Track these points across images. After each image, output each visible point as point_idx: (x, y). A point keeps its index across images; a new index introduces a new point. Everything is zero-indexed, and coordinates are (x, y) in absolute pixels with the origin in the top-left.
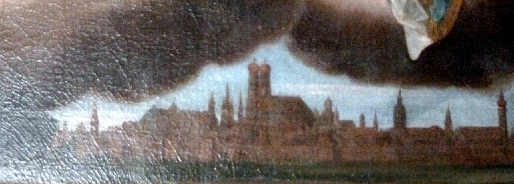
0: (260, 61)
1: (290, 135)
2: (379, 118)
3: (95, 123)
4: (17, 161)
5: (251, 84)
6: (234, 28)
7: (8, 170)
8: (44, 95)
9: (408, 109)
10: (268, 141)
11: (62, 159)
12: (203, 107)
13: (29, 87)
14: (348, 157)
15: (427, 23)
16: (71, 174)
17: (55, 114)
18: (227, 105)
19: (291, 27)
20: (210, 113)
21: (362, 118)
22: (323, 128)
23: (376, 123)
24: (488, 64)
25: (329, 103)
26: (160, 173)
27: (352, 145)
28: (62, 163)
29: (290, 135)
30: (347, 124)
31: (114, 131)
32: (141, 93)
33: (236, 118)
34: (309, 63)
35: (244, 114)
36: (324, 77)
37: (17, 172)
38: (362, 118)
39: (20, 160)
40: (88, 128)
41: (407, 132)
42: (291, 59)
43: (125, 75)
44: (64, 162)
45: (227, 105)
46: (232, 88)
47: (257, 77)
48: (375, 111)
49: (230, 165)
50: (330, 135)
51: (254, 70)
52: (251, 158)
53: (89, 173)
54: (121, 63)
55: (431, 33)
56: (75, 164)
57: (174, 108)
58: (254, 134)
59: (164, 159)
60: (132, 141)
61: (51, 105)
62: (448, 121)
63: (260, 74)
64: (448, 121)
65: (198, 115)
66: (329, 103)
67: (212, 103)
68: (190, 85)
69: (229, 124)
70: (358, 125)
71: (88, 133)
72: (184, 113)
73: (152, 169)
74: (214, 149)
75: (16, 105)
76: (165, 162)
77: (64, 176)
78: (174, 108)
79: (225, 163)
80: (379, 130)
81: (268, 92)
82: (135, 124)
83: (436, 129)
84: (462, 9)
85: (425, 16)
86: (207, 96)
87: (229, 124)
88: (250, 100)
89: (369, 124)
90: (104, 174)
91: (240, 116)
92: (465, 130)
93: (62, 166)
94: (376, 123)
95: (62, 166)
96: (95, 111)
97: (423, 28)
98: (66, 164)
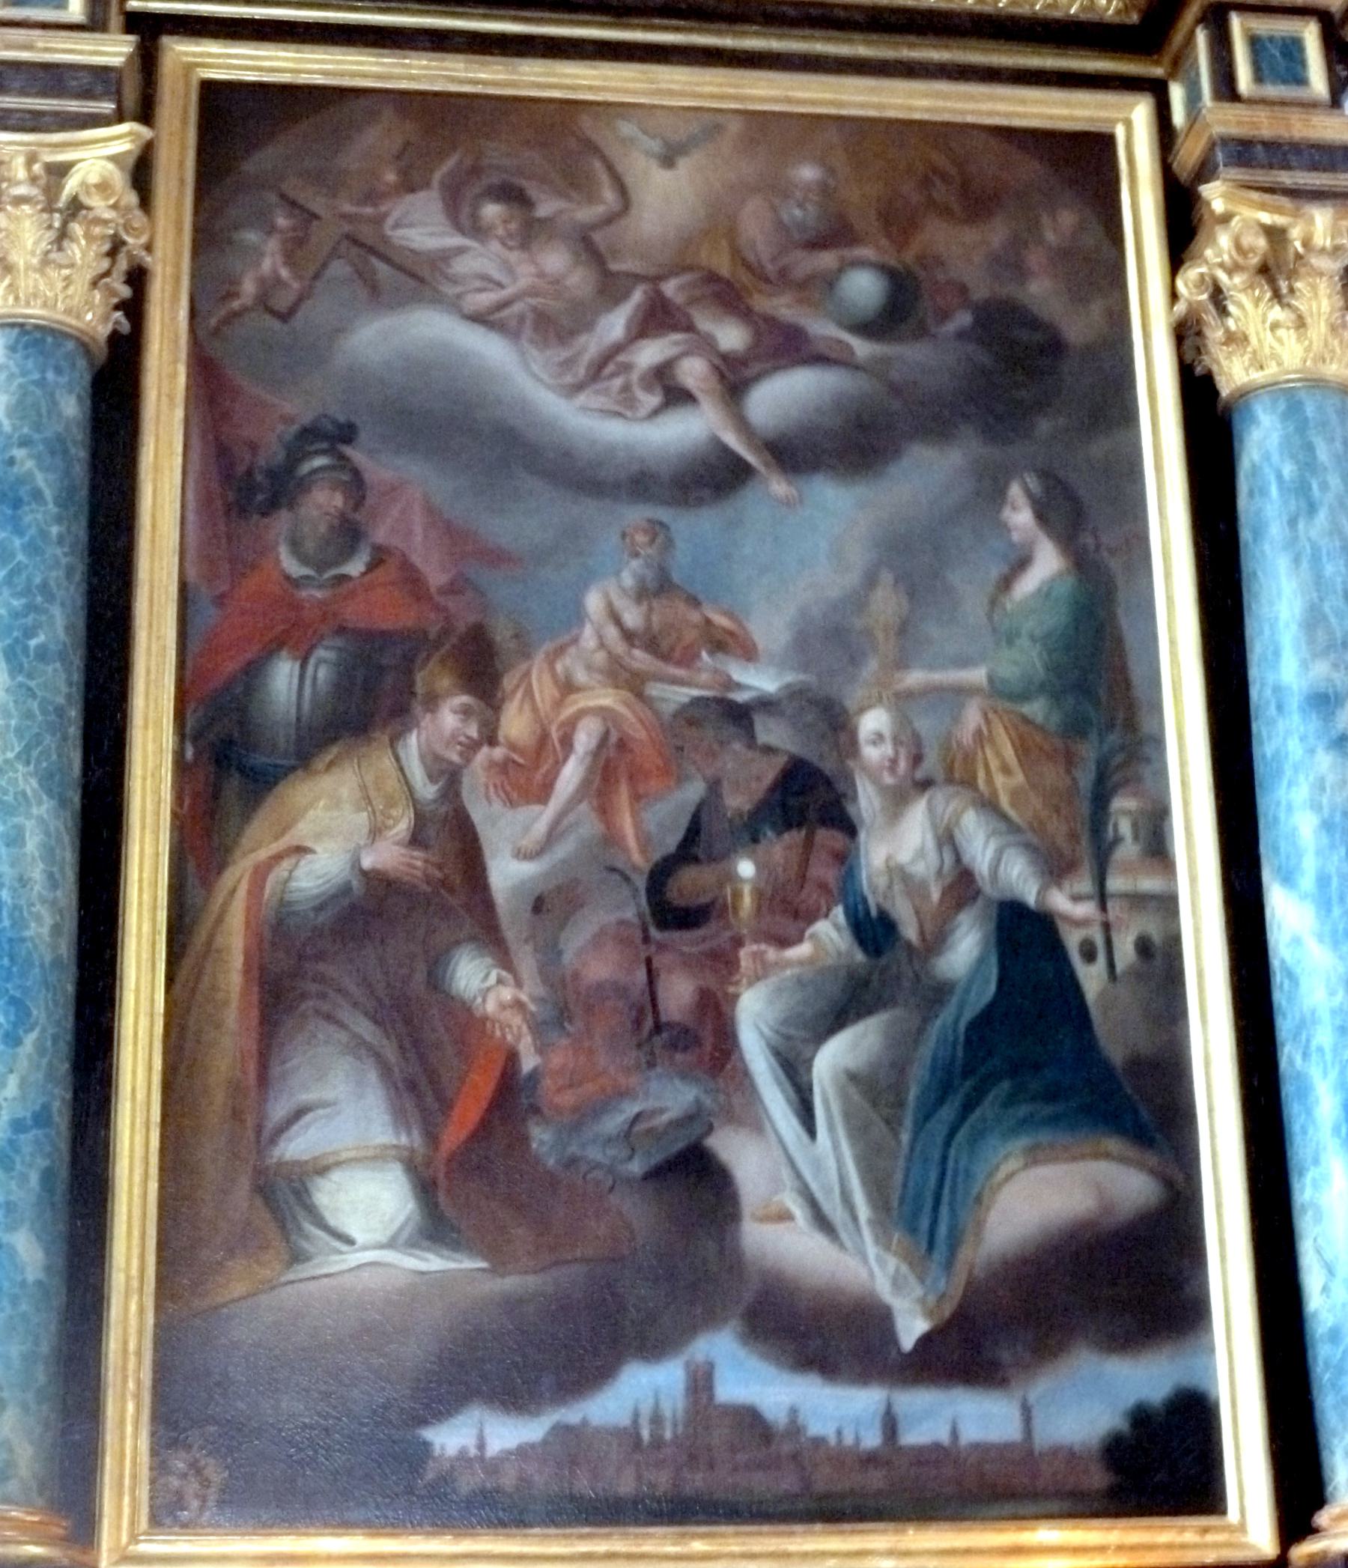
0: (700, 1357)
1: (742, 1457)
2: (862, 1433)
3: (481, 1446)
4: (379, 1499)
5: (687, 1389)
6: (1292, 122)
7: (332, 994)
8: (414, 1409)
9: (900, 1418)
10: (711, 1466)
11: (436, 1496)
12: (625, 1421)
13: (395, 1400)
14: (820, 1486)
15: (922, 1301)
16: (450, 1516)
17: (429, 1434)
18: (656, 1419)
19: (740, 1309)
20: (632, 1431)
21: (839, 1433)
22: (787, 1448)
23: (858, 1439)
24: (1005, 1356)
25: (793, 1411)
26: (567, 1514)
27: (826, 1470)
28: (437, 1500)
29: (742, 1457)
30: (819, 1442)
31: (506, 1455)
32: (795, 693)
33: (668, 1435)
34: (765, 1356)
35: (680, 1429)
36: (786, 1376)
37: (378, 1513)
38: (839, 1433)
39: (384, 1498)
40: (473, 1452)
41: (900, 1450)
42: (741, 1353)
43: (519, 1380)
44: (440, 1499)
45: (656, 1419)
46: (662, 1397)
47: (695, 1381)
48: (857, 1422)
49: (659, 1502)
50: (795, 1457)
51: (692, 1368)
52: (688, 1490)
53: (472, 1514)
54: (515, 1364)
55: (929, 1314)
56: (455, 1502)
57: (585, 1423)
58: (693, 1458)
59: (571, 1494)
60: (531, 1469)
61: (424, 1422)
62: (955, 1434)
63: (700, 1373)
64: (955, 1434)
65: (618, 1433)
66: (793, 1411)
67: (636, 1416)
68: (767, 1060)
69: (657, 1443)
70: (832, 1441)
71: (471, 1459)
72: (597, 1430)
73: (556, 1507)
74: (639, 1478)
75: (377, 1424)
76: (572, 1498)
77: (439, 1519)
78: (585, 1423)
79: (653, 1498)
80: (861, 1449)
81: (711, 1397)
82: (533, 1446)
83: (937, 1447)
84: (969, 1283)
85: (919, 1291)
86: (629, 1405)
87: (657, 1443)
88: (687, 1412)
89: (849, 1440)
90: (492, 1515)
91: (675, 1433)
92: (976, 1446)
93: (437, 1504)
94: (858, 1439)
95: (437, 1504)
96: (481, 1431)
97: (918, 1308)
98: (442, 1501)
